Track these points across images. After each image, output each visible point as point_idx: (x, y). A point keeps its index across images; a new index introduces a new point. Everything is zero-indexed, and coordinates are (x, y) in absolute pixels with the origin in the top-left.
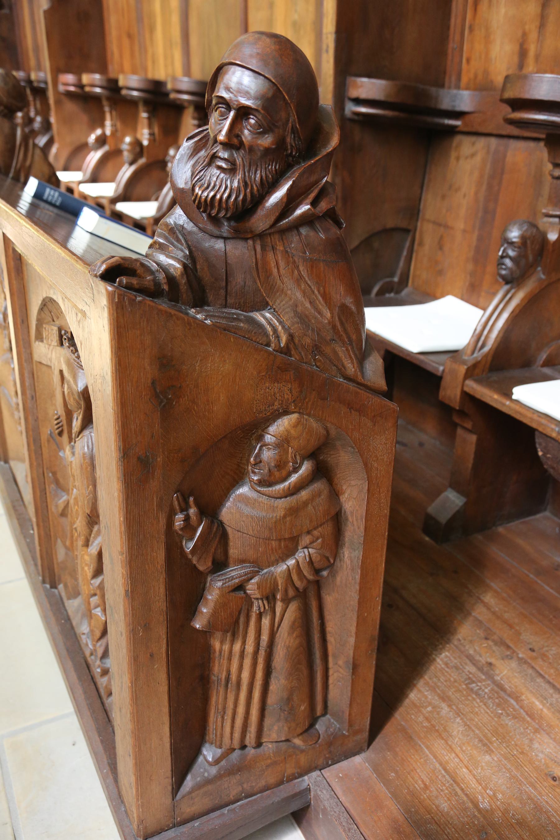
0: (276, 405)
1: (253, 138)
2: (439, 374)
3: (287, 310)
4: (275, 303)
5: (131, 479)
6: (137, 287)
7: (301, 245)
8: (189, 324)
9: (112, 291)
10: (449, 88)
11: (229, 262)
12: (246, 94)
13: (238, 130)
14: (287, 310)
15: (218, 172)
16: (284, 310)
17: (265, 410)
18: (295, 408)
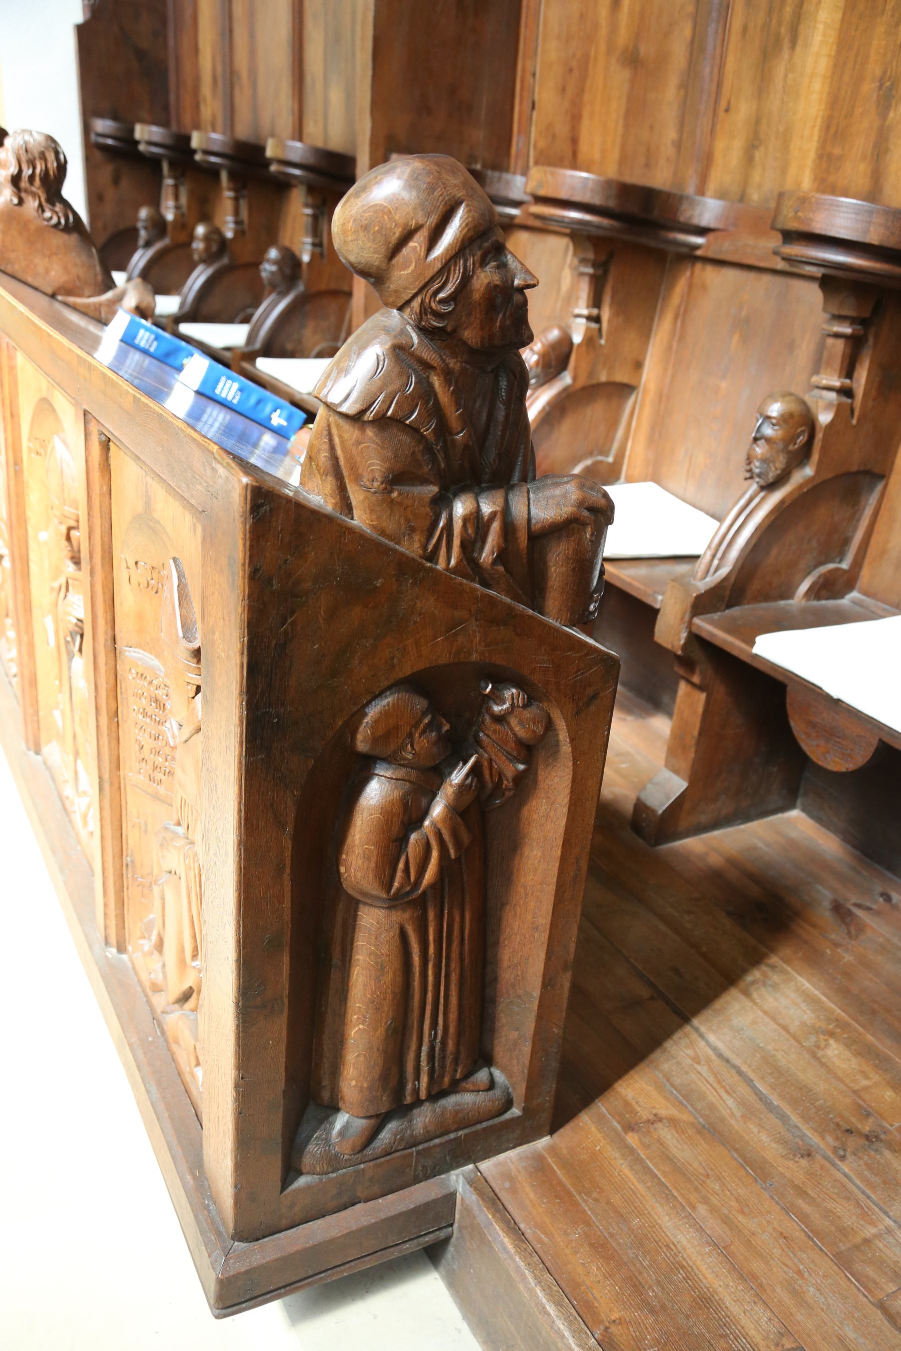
2: (657, 606)
10: (514, 173)
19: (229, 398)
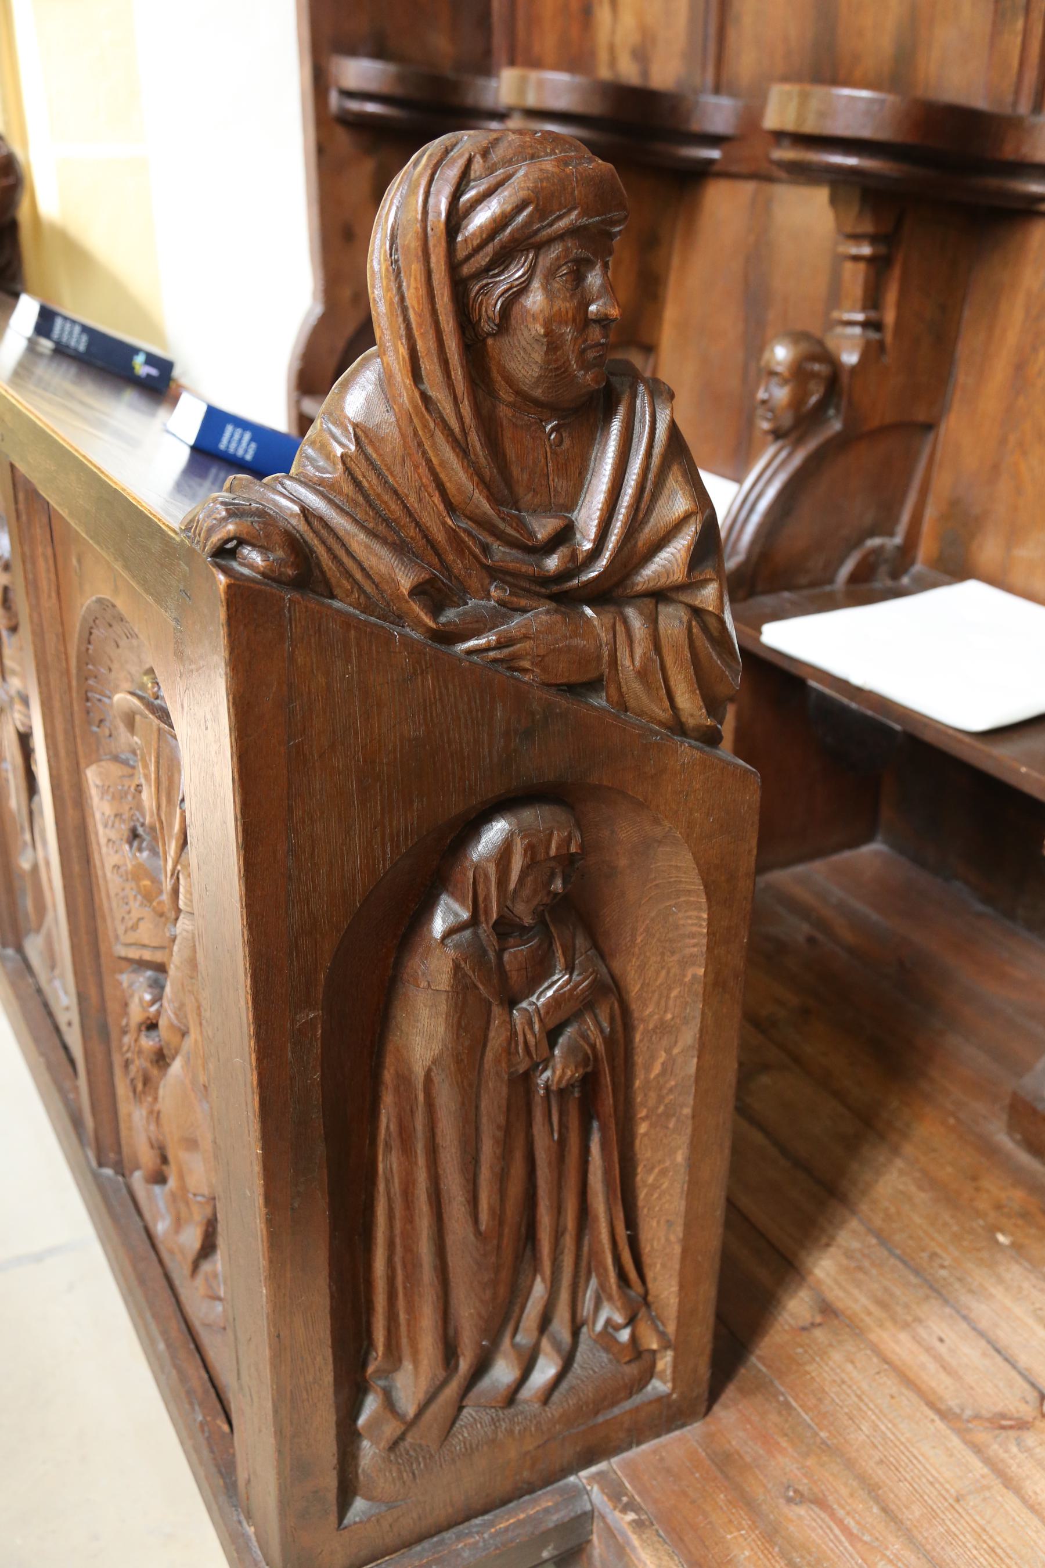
19: (240, 453)
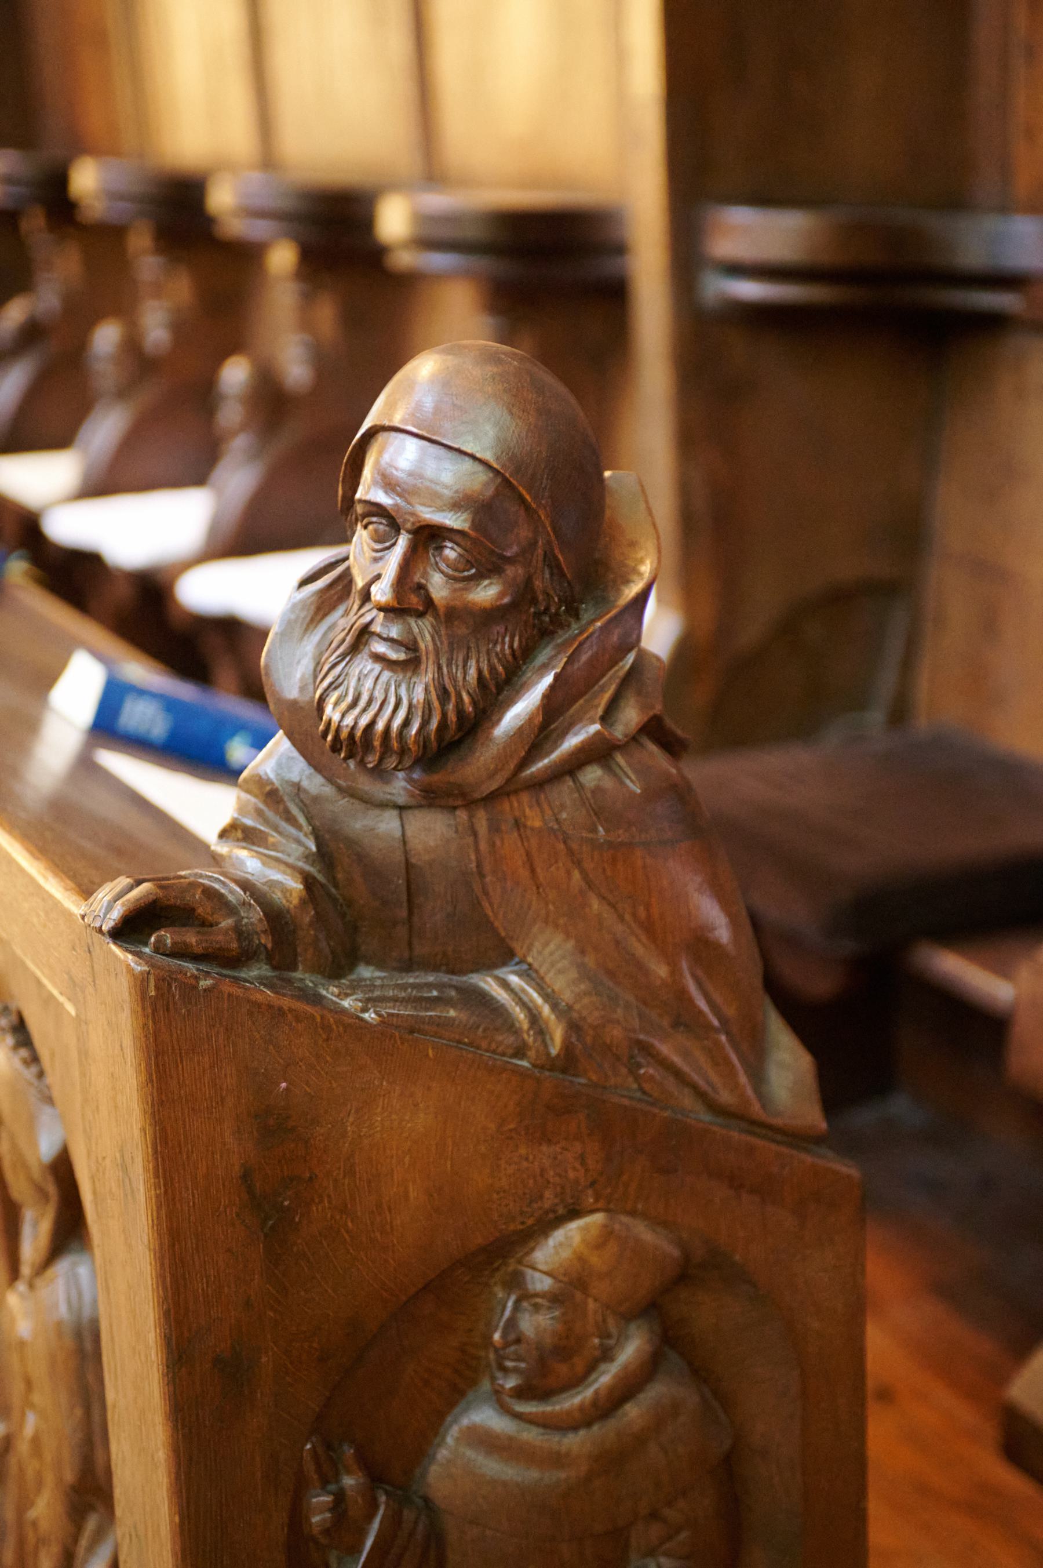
0: (549, 1198)
1: (455, 590)
3: (560, 965)
4: (529, 949)
5: (197, 1415)
6: (198, 950)
7: (584, 812)
8: (326, 1027)
9: (142, 973)
11: (413, 861)
12: (433, 498)
13: (418, 575)
14: (560, 965)
15: (378, 667)
16: (552, 965)
17: (522, 1213)
18: (597, 1200)
